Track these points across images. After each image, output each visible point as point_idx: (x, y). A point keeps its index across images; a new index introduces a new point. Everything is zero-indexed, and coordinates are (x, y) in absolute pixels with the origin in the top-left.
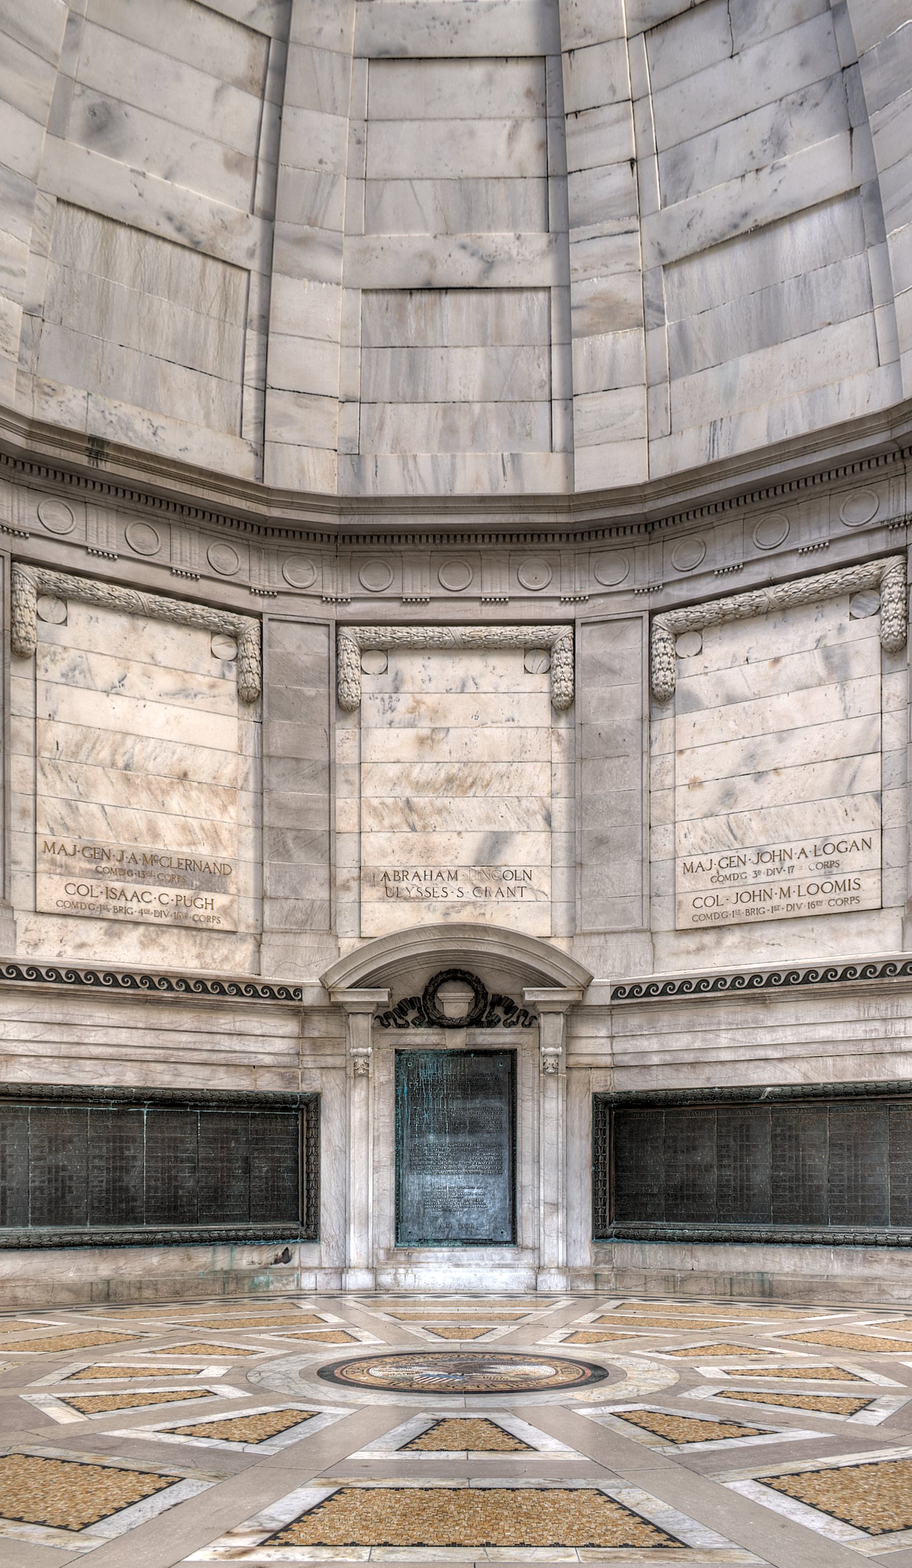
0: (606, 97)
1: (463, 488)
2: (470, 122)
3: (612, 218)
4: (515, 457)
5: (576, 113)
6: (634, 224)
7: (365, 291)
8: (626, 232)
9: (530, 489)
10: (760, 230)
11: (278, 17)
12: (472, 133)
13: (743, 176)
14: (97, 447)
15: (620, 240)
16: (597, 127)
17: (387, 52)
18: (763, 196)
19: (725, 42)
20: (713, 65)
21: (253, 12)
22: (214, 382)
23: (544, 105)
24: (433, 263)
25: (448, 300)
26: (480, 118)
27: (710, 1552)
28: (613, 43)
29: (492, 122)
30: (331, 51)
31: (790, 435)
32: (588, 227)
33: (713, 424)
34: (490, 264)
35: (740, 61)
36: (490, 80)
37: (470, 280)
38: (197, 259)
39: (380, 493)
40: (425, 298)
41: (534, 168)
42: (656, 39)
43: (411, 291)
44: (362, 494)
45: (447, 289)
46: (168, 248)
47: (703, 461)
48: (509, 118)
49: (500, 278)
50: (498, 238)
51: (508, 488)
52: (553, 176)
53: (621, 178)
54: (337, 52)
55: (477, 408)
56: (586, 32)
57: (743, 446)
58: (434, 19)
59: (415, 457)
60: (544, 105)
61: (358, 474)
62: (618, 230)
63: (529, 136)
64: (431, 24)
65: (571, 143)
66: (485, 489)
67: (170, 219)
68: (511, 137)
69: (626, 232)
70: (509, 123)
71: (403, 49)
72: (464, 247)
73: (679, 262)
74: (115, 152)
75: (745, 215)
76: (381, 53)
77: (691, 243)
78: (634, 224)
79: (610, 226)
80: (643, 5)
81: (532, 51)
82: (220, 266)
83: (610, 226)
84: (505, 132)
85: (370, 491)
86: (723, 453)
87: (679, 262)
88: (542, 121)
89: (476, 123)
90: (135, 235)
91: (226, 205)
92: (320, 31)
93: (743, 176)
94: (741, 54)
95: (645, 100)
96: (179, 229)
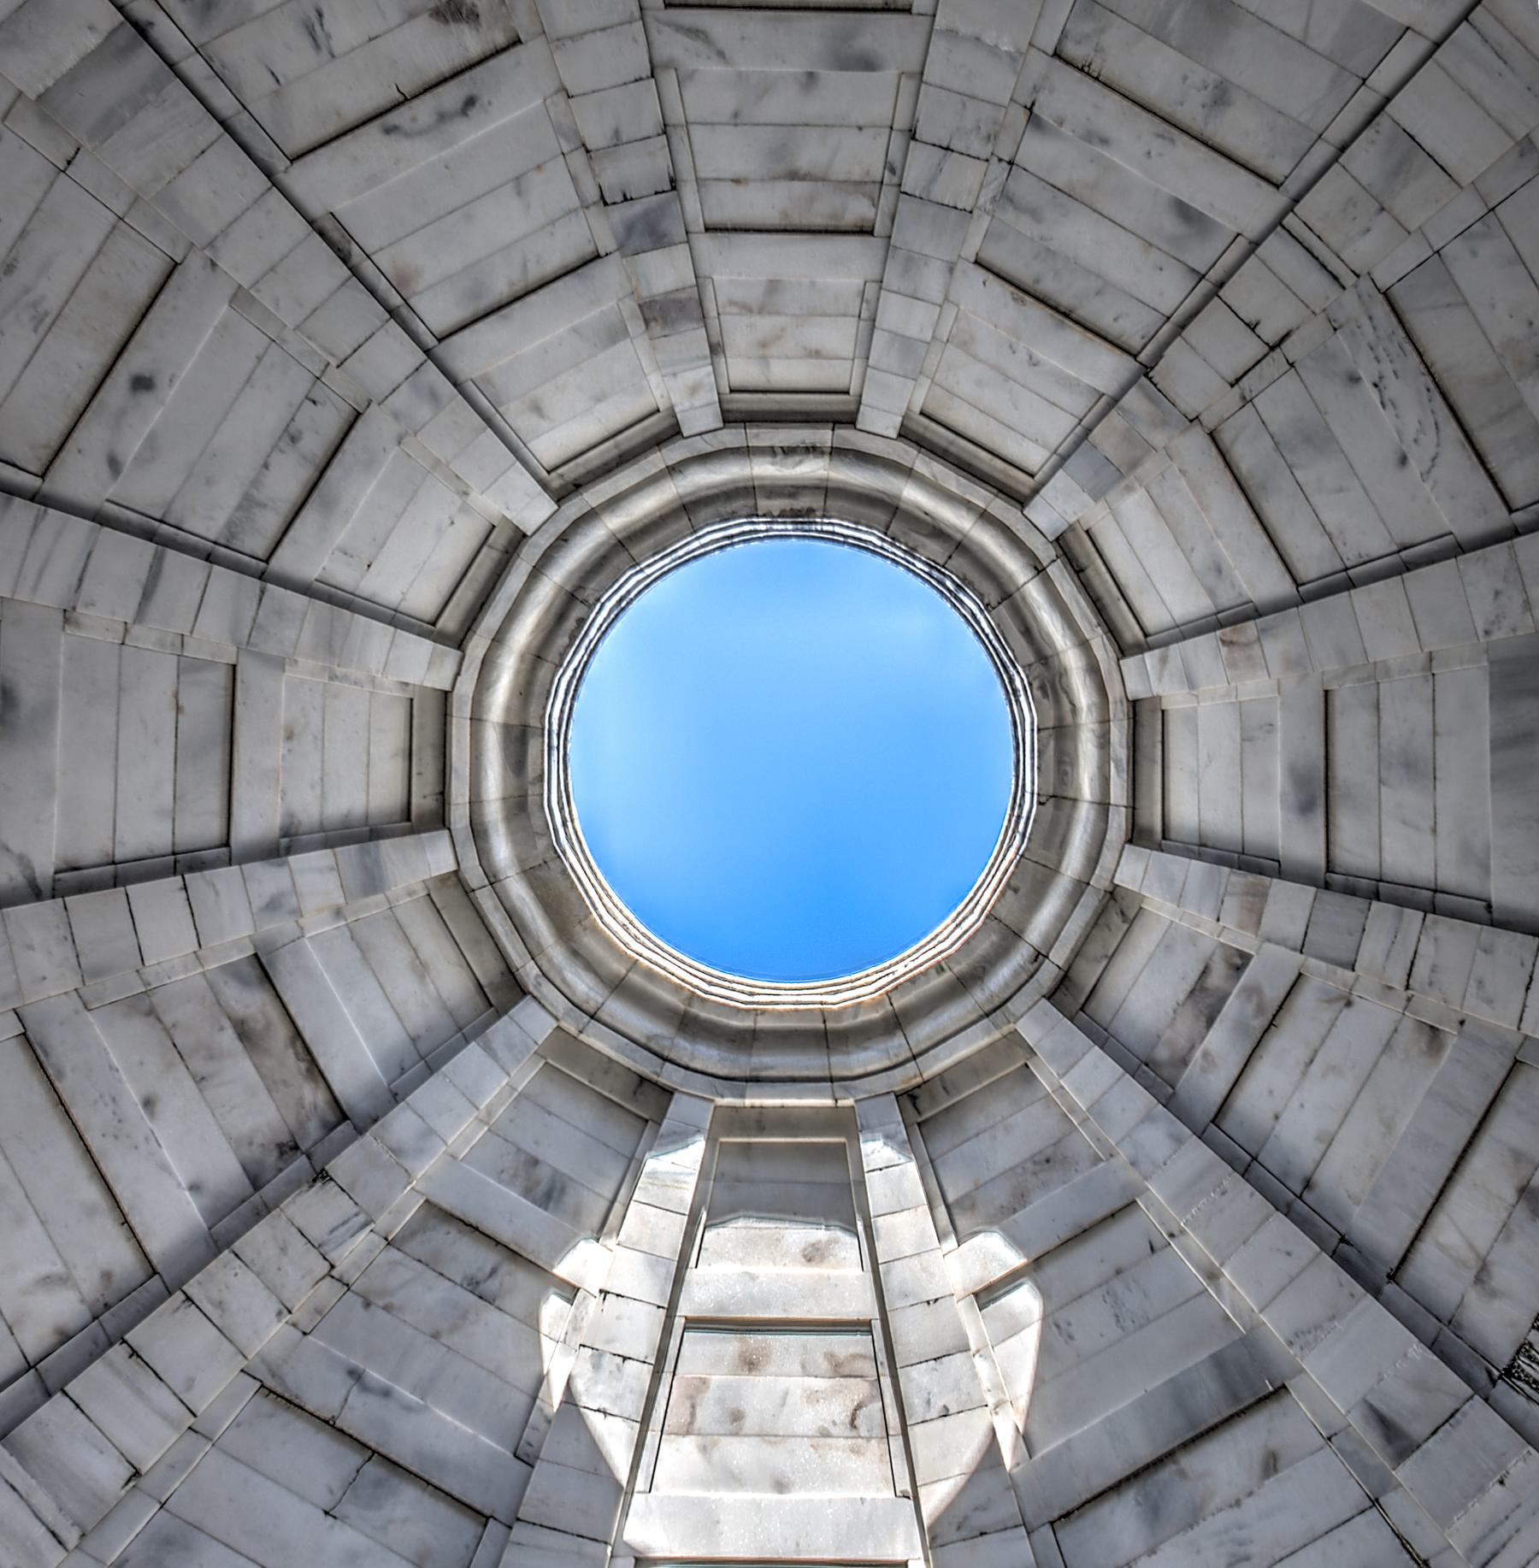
0: (177, 1383)
2: (31, 1211)
3: (56, 1497)
5: (134, 1353)
6: (71, 1538)
8: (54, 1534)
11: (14, 888)
12: (19, 1221)
15: (39, 1532)
16: (139, 1393)
17: (46, 1054)
19: (331, 1491)
20: (303, 1498)
21: (8, 850)
23: (107, 1307)
26: (42, 1223)
27: (164, 1167)
28: (231, 1349)
29: (48, 1243)
30: (15, 969)
32: (20, 1468)
34: (1221, 96)
35: (332, 1527)
36: (91, 1212)
41: (34, 1339)
42: (267, 1405)
48: (65, 1264)
52: (39, 1375)
53: (107, 1473)
54: (18, 981)
56: (220, 1305)
58: (114, 1099)
60: (107, 1307)
62: (49, 1518)
63: (64, 1307)
64: (107, 1099)
65: (97, 1367)
68: (48, 1281)
69: (54, 1534)
70: (59, 1268)
71: (60, 1074)
76: (41, 1047)
78: (71, 1538)
79: (42, 1500)
80: (285, 1361)
81: (154, 1248)
83: (42, 1500)
84: (47, 1269)
88: (88, 1316)
89: (34, 1218)
91: (524, 110)
92: (31, 947)
94: (338, 1522)
95: (203, 1441)
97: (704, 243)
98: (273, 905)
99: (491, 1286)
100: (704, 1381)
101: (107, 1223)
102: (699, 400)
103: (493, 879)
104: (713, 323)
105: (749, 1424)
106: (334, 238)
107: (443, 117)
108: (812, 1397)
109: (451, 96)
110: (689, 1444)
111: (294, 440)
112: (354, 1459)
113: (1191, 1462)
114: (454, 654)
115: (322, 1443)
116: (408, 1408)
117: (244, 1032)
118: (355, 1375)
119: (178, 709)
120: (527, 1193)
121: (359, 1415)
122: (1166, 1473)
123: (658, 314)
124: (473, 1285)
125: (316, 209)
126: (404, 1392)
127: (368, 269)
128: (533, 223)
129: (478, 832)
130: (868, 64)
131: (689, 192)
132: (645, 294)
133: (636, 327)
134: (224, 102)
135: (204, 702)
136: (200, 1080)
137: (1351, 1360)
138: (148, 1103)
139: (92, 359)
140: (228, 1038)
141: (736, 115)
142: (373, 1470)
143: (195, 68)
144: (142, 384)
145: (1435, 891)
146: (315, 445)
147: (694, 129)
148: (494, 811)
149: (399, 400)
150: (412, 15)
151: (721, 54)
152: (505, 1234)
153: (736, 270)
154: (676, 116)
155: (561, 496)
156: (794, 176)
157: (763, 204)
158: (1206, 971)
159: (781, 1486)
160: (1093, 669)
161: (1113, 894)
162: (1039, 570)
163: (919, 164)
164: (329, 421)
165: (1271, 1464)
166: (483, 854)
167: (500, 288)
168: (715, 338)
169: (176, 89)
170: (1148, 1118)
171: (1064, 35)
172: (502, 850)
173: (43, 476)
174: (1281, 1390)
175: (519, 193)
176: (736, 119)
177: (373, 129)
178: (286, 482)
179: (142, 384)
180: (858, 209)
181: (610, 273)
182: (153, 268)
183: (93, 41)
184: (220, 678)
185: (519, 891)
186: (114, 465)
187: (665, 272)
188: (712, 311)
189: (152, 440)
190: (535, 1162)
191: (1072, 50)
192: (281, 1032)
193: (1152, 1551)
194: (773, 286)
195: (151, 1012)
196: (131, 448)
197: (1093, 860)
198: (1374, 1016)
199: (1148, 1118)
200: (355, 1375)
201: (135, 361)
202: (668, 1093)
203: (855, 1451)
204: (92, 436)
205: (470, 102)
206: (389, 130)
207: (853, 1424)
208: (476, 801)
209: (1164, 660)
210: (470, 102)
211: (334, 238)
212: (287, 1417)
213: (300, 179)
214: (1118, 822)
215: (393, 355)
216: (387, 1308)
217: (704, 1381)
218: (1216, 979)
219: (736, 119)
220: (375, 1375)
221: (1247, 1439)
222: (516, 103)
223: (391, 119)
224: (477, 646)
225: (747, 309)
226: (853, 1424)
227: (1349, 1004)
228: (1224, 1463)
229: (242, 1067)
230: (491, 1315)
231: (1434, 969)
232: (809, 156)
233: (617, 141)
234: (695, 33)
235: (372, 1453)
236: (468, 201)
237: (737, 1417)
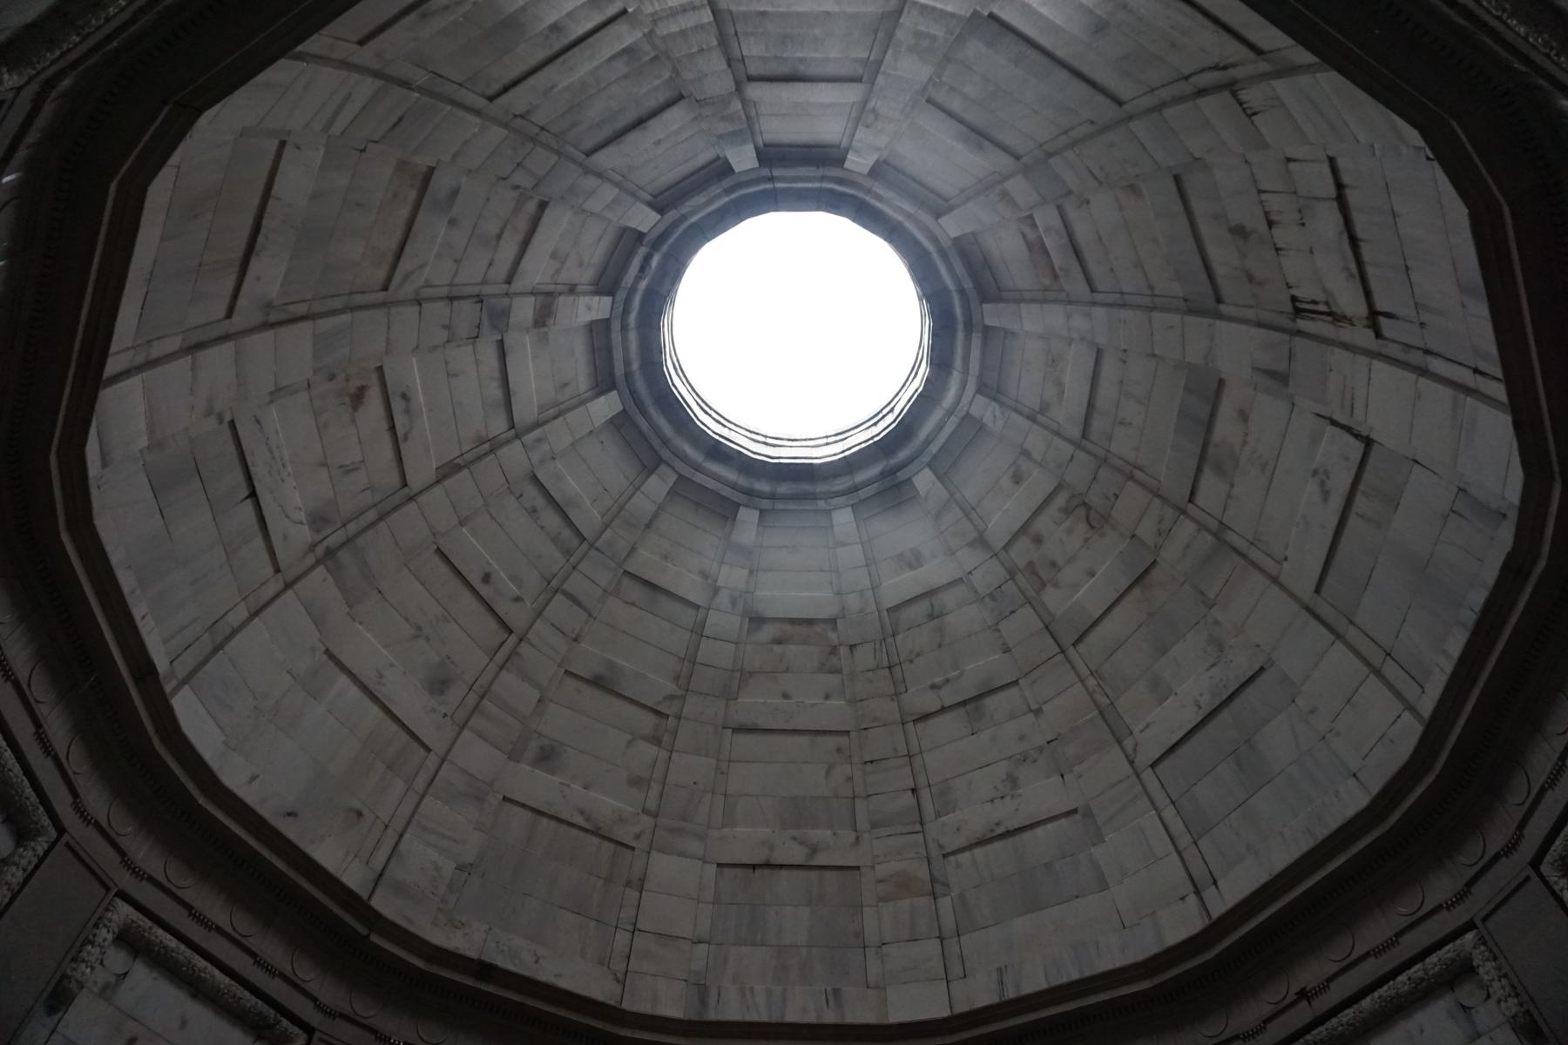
1: (792, 1017)
4: (836, 992)
7: (719, 865)
9: (849, 1019)
10: (1009, 834)
13: (1277, 250)
14: (485, 970)
18: (1008, 814)
22: (593, 924)
24: (771, 848)
25: (784, 872)
27: (813, 705)
31: (1065, 980)
33: (999, 970)
34: (814, 850)
37: (799, 860)
38: (595, 840)
39: (720, 1017)
40: (767, 872)
43: (754, 867)
44: (705, 1018)
45: (781, 866)
46: (575, 832)
47: (996, 1000)
49: (821, 859)
50: (819, 834)
51: (830, 1017)
55: (804, 952)
56: (875, 719)
57: (1029, 988)
59: (752, 989)
61: (703, 1003)
66: (811, 1018)
67: (582, 813)
72: (794, 839)
73: (954, 853)
74: (552, 772)
75: (998, 824)
77: (962, 841)
82: (612, 846)
85: (712, 1016)
86: (1011, 994)
87: (954, 853)
90: (553, 823)
93: (1277, 250)
96: (587, 820)
97: (517, 285)
98: (734, 602)
101: (820, 739)
102: (595, 306)
106: (447, 471)
107: (407, 411)
109: (398, 405)
110: (1049, 589)
111: (535, 511)
114: (663, 467)
116: (958, 677)
117: (779, 641)
118: (933, 687)
119: (633, 604)
121: (949, 697)
123: (543, 318)
125: (434, 478)
128: (473, 368)
129: (750, 493)
130: (455, 193)
131: (487, 290)
134: (371, 515)
135: (635, 592)
136: (787, 670)
138: (785, 696)
140: (777, 649)
142: (970, 707)
143: (352, 528)
144: (487, 578)
145: (1066, 132)
146: (540, 502)
147: (456, 281)
148: (742, 481)
149: (535, 457)
150: (354, 421)
152: (917, 591)
153: (537, 270)
154: (444, 291)
156: (499, 237)
157: (508, 249)
158: (1024, 236)
162: (771, 179)
163: (521, 178)
164: (531, 491)
165: (1244, 416)
169: (360, 541)
170: (1069, 317)
171: (483, 95)
173: (511, 632)
175: (456, 375)
176: (458, 261)
178: (551, 519)
179: (487, 578)
180: (531, 207)
181: (510, 340)
182: (436, 560)
183: (331, 580)
184: (626, 581)
186: (518, 599)
187: (524, 310)
188: (551, 288)
189: (513, 579)
190: (901, 555)
191: (491, 92)
192: (788, 627)
194: (554, 255)
195: (751, 674)
199: (1069, 317)
200: (933, 687)
205: (404, 396)
206: (406, 438)
207: (1092, 527)
208: (734, 486)
210: (404, 396)
211: (447, 471)
212: (931, 722)
213: (416, 482)
215: (514, 455)
218: (1031, 236)
219: (458, 261)
220: (938, 680)
221: (1227, 410)
222: (412, 374)
223: (400, 434)
224: (665, 454)
225: (558, 271)
226: (1092, 527)
228: (1226, 428)
229: (792, 650)
232: (492, 228)
233: (447, 327)
234: (406, 277)
235: (964, 703)
236: (447, 392)
237: (1053, 564)
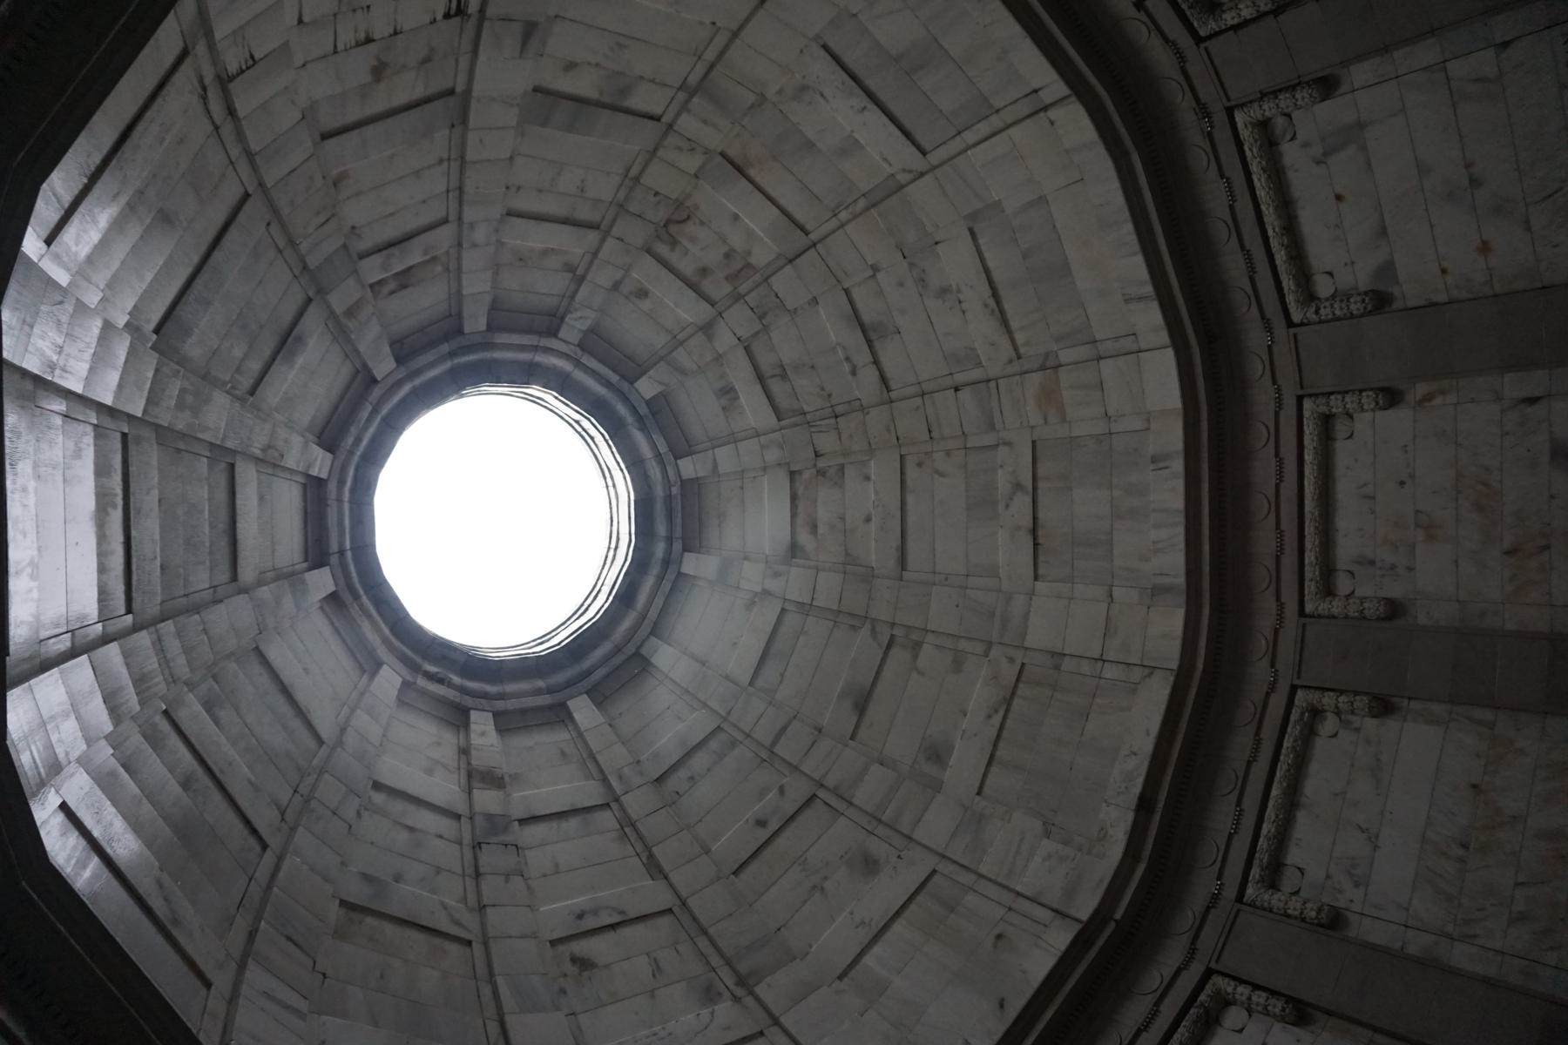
27: (876, 492)
98: (777, 575)
99: (778, 371)
100: (727, 278)
103: (670, 540)
104: (463, 765)
105: (726, 249)
106: (655, 868)
107: (595, 912)
108: (693, 240)
109: (590, 923)
111: (692, 778)
112: (877, 344)
113: (593, 94)
115: (883, 359)
116: (844, 348)
117: (814, 528)
118: (854, 373)
119: (782, 675)
120: (737, 398)
122: (606, 99)
123: (494, 780)
124: (784, 376)
126: (841, 354)
127: (639, 848)
128: (548, 848)
129: (666, 563)
130: (367, 878)
131: (467, 839)
132: (501, 793)
133: (507, 779)
134: (703, 943)
137: (501, 76)
139: (781, 842)
140: (820, 531)
141: (438, 873)
143: (715, 961)
144: (761, 823)
145: (280, 252)
150: (607, 966)
151: (445, 908)
154: (470, 883)
155: (563, 706)
156: (411, 829)
158: (392, 293)
159: (736, 217)
160: (341, 482)
161: (400, 360)
165: (570, 66)
166: (669, 551)
167: (572, 824)
168: (463, 757)
171: (261, 857)
172: (660, 550)
174: (536, 89)
176: (438, 870)
177: (632, 915)
178: (700, 761)
179: (761, 823)
180: (379, 798)
181: (518, 812)
185: (661, 529)
186: (782, 791)
187: (487, 800)
188: (463, 773)
192: (800, 520)
193: (641, 78)
195: (847, 554)
196: (772, 795)
197: (399, 384)
198: (354, 213)
200: (854, 373)
201: (763, 834)
202: (648, 403)
203: (697, 207)
204: (790, 807)
205: (580, 916)
206: (622, 913)
209: (309, 466)
210: (580, 916)
211: (655, 868)
214: (376, 392)
215: (635, 803)
216: (823, 389)
217: (727, 278)
218: (392, 285)
220: (847, 368)
221: (566, 84)
227: (353, 228)
228: (583, 84)
230: (786, 360)
231: (318, 213)
233: (507, 876)
234: (457, 923)
235: (869, 342)
237: (727, 256)
